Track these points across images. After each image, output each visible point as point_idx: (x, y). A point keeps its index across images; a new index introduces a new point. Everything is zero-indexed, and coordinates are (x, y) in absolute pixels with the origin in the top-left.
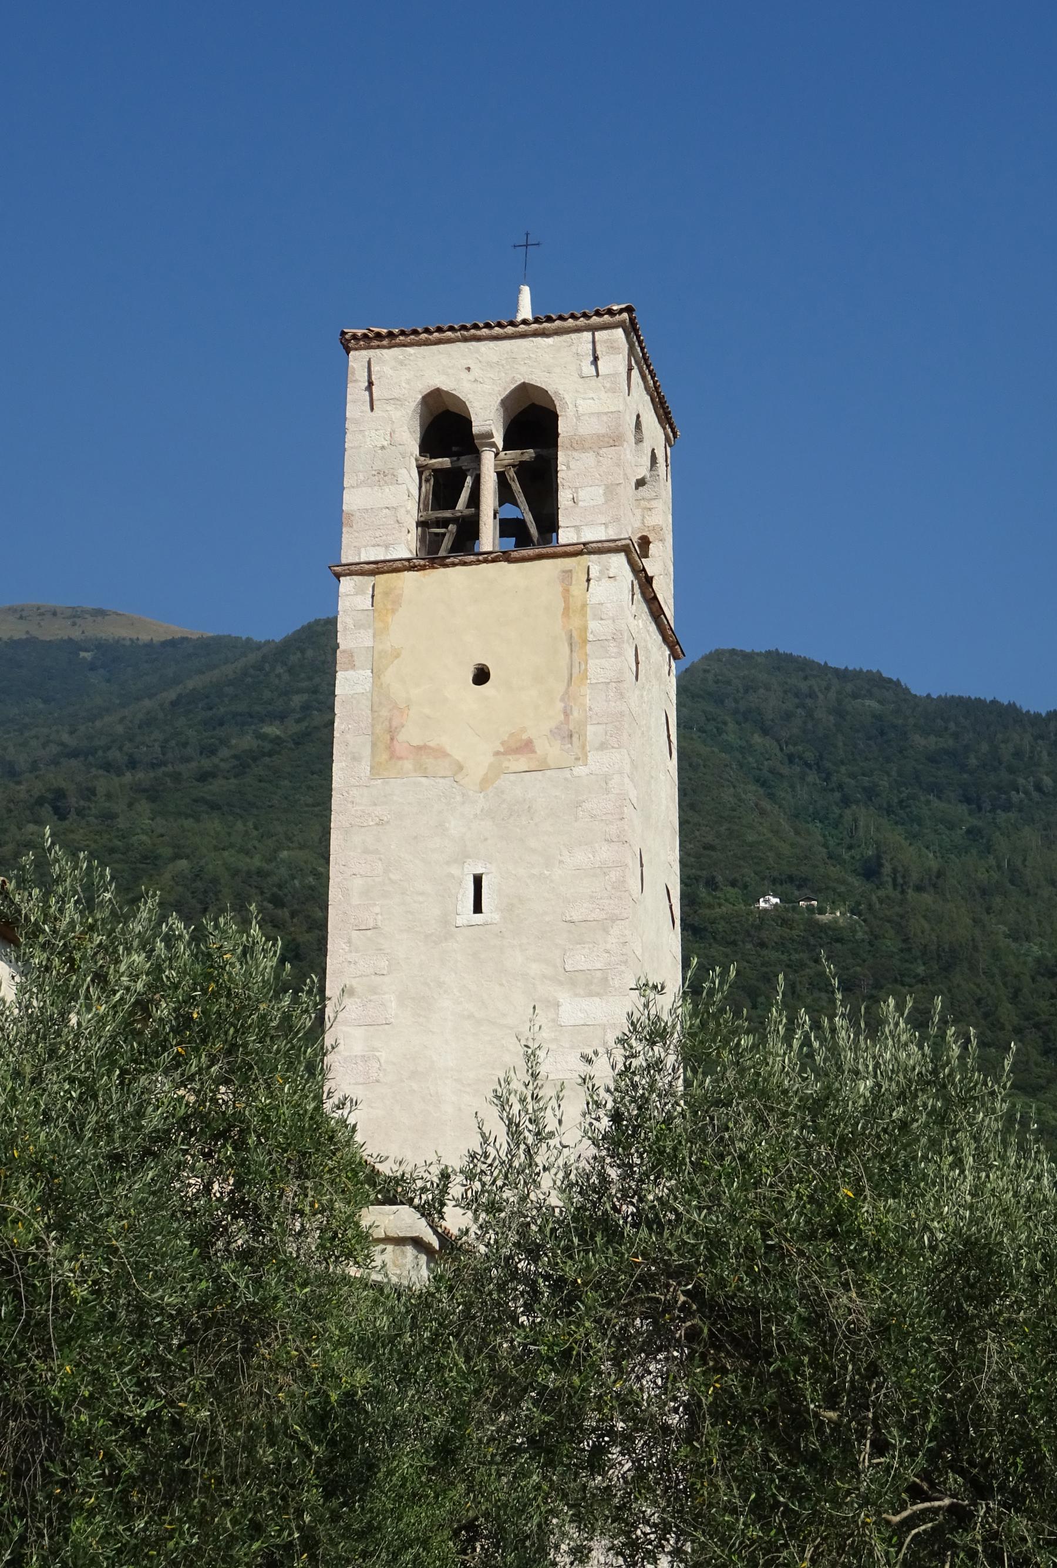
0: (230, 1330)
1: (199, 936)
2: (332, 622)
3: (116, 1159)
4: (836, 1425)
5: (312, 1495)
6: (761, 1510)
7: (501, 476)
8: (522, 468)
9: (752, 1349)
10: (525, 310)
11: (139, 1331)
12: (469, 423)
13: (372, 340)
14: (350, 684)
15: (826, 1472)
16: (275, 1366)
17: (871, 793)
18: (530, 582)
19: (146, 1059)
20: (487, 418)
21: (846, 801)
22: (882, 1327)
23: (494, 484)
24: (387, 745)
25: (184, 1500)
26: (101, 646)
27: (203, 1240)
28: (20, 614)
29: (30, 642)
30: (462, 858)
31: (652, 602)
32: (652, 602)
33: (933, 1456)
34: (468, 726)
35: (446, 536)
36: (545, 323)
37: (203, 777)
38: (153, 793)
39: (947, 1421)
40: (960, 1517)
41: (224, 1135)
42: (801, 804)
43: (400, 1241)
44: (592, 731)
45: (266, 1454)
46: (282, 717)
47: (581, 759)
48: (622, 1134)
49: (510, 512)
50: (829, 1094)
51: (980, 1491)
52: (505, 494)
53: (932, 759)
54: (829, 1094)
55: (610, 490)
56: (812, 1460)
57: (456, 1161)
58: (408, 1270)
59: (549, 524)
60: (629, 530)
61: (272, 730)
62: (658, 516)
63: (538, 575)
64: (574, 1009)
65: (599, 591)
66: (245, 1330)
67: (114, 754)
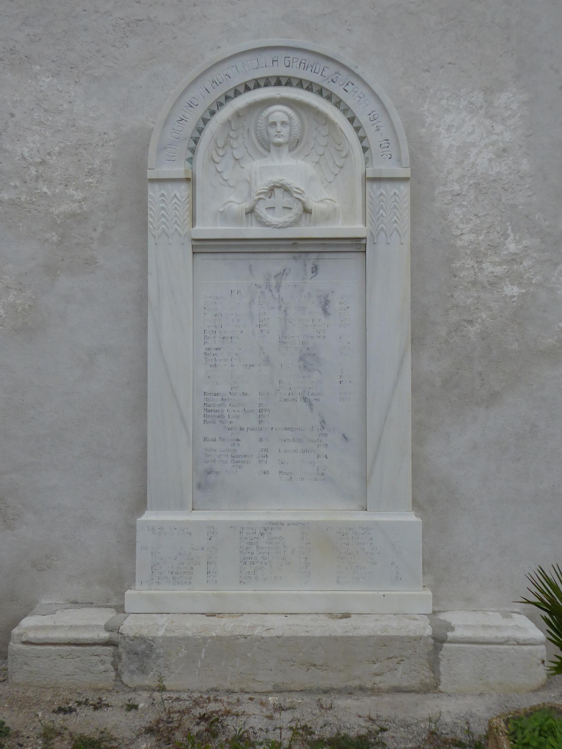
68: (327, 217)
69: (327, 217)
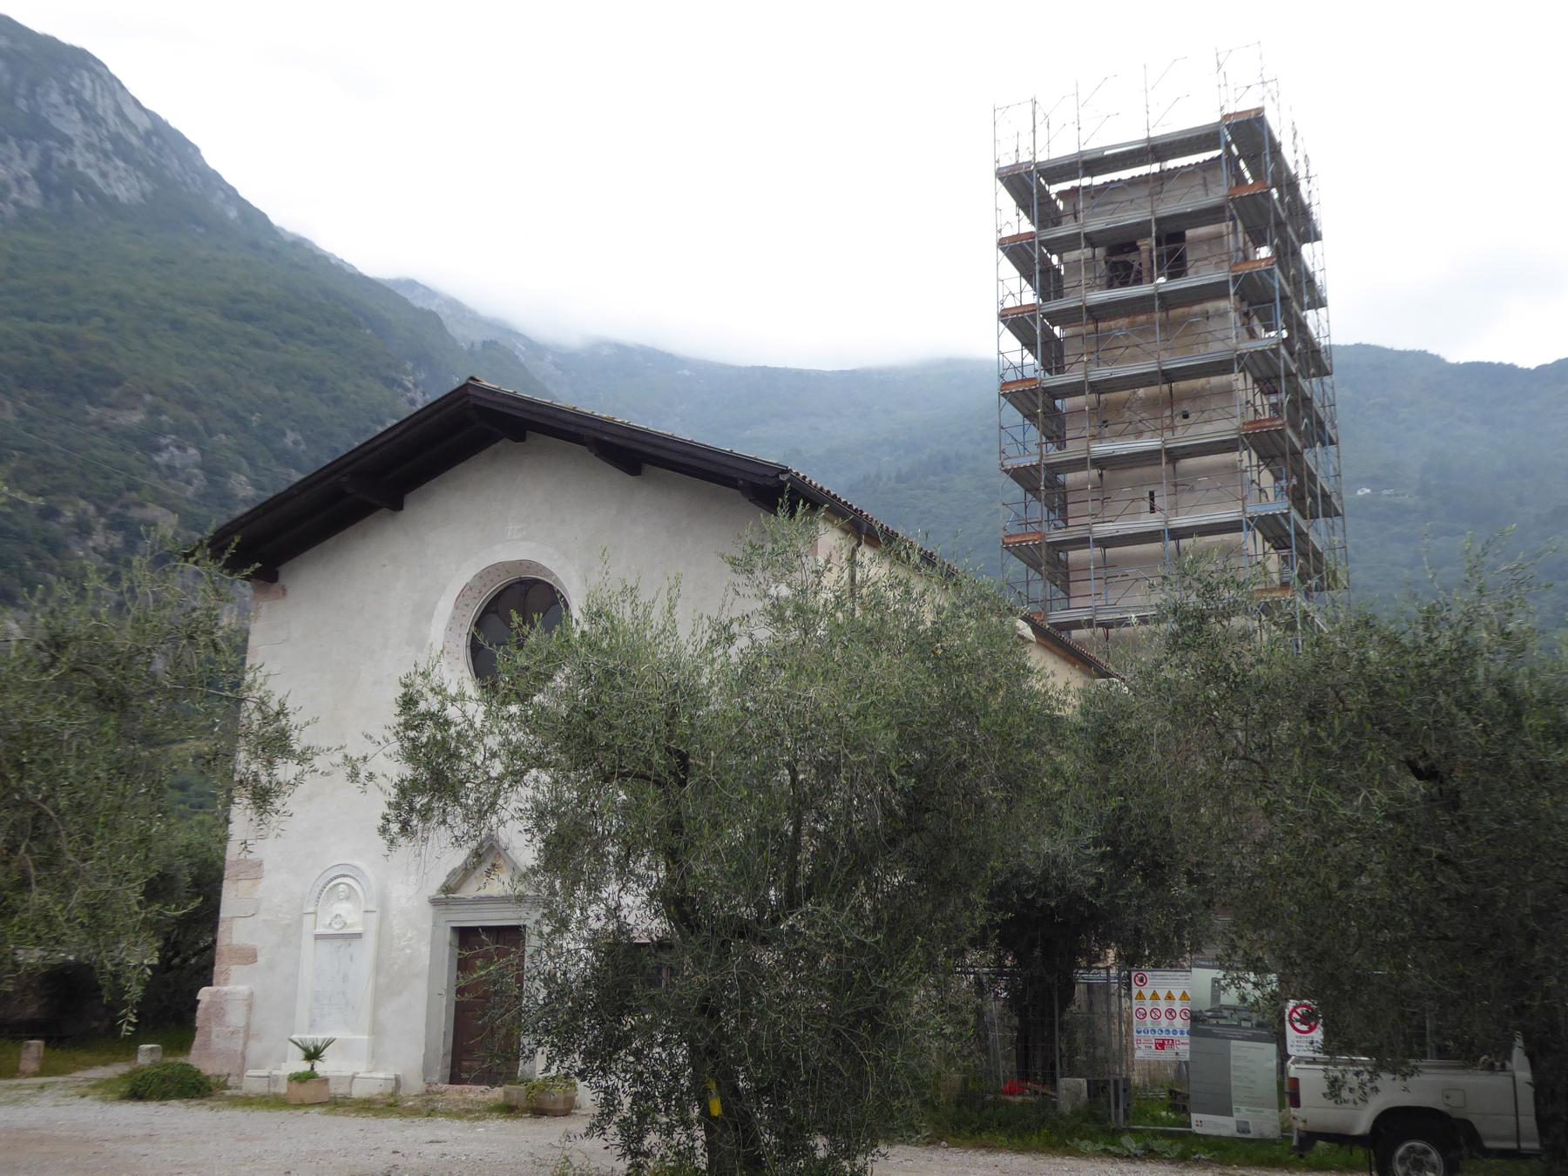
68: (352, 926)
69: (352, 926)
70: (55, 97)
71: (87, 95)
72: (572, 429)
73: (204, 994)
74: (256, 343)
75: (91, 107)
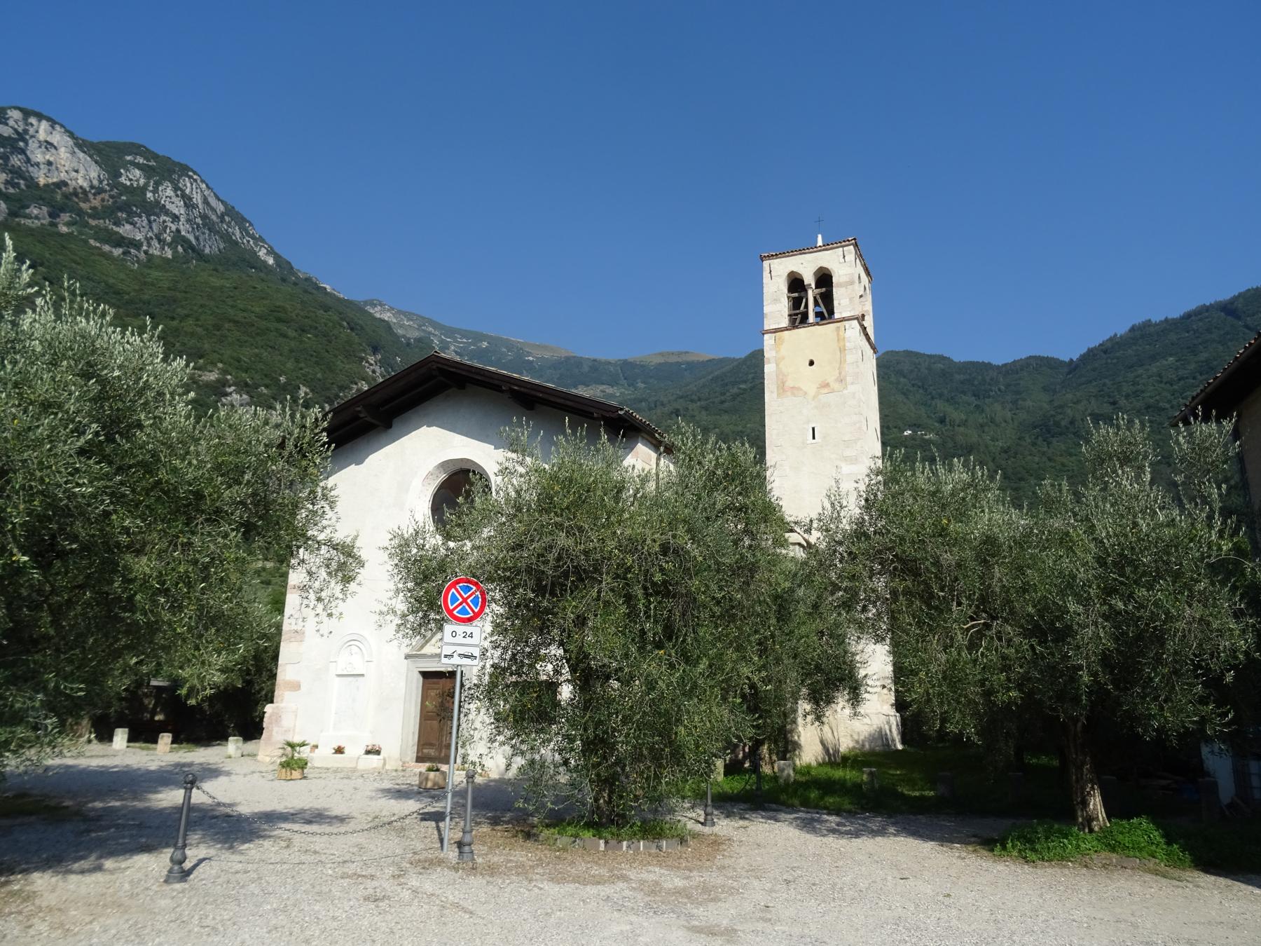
0: (746, 570)
1: (729, 448)
2: (762, 351)
3: (708, 518)
4: (944, 597)
5: (773, 621)
6: (920, 624)
7: (815, 298)
8: (821, 295)
9: (916, 573)
10: (820, 243)
11: (718, 571)
12: (802, 281)
13: (770, 257)
14: (769, 369)
15: (941, 612)
16: (761, 581)
17: (941, 395)
18: (826, 331)
19: (715, 487)
20: (809, 279)
21: (933, 398)
22: (959, 565)
23: (813, 301)
24: (782, 388)
25: (734, 622)
26: (688, 363)
27: (736, 543)
28: (662, 354)
29: (666, 363)
30: (808, 422)
31: (867, 335)
32: (867, 335)
33: (978, 607)
34: (807, 379)
35: (798, 319)
36: (827, 246)
37: (722, 402)
38: (706, 408)
39: (981, 595)
40: (987, 626)
41: (740, 510)
42: (920, 400)
43: (794, 544)
44: (849, 379)
45: (758, 609)
46: (745, 382)
47: (846, 388)
48: (869, 505)
49: (818, 309)
50: (938, 491)
51: (994, 618)
52: (816, 304)
53: (962, 382)
54: (938, 491)
55: (851, 299)
56: (936, 608)
57: (814, 516)
58: (800, 554)
59: (831, 312)
60: (858, 313)
61: (743, 386)
62: (867, 307)
63: (828, 329)
64: (846, 469)
65: (849, 333)
66: (750, 570)
67: (694, 397)
70: (169, 192)
71: (188, 191)
72: (496, 382)
73: (269, 708)
74: (285, 336)
75: (190, 199)
